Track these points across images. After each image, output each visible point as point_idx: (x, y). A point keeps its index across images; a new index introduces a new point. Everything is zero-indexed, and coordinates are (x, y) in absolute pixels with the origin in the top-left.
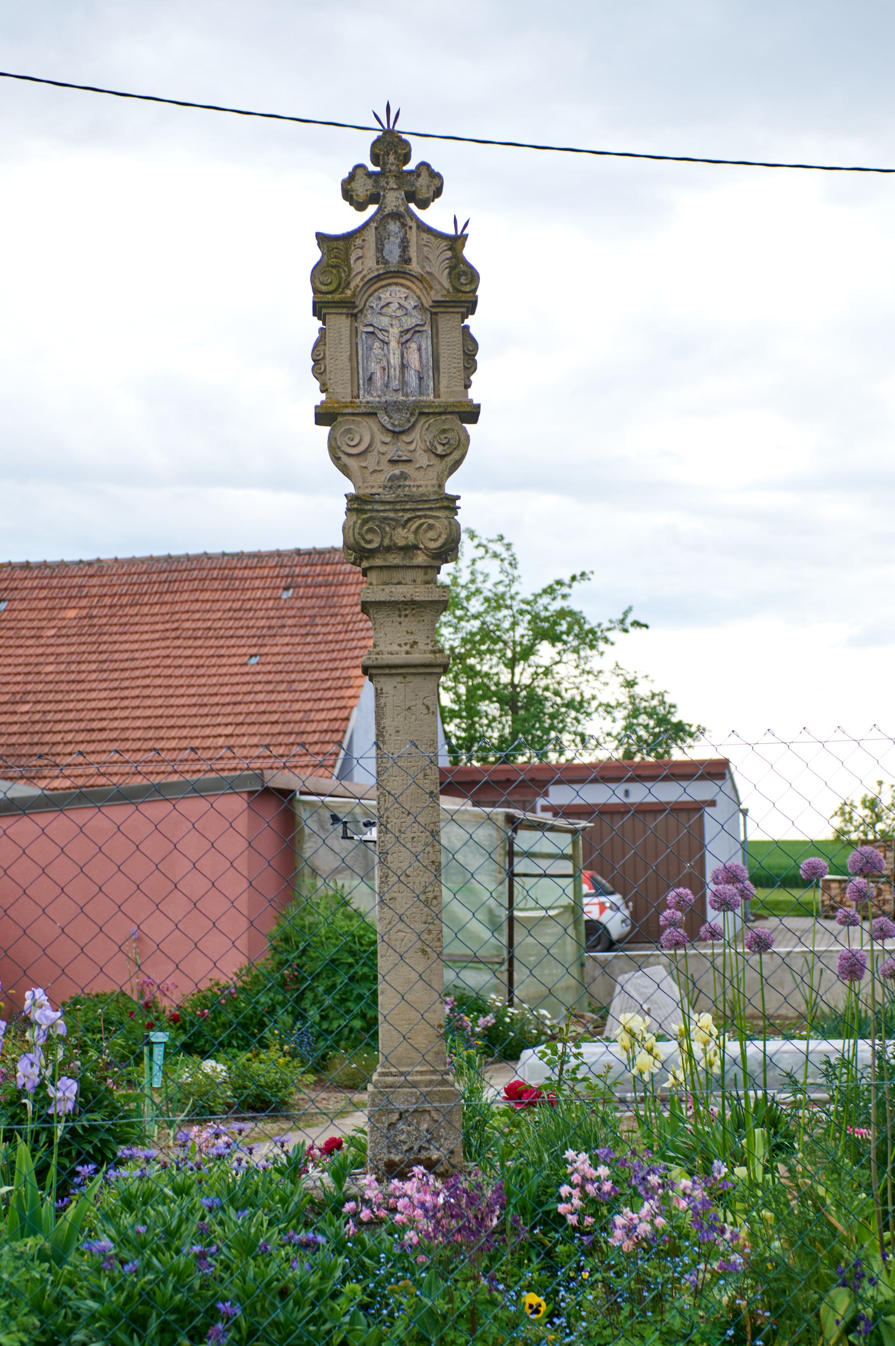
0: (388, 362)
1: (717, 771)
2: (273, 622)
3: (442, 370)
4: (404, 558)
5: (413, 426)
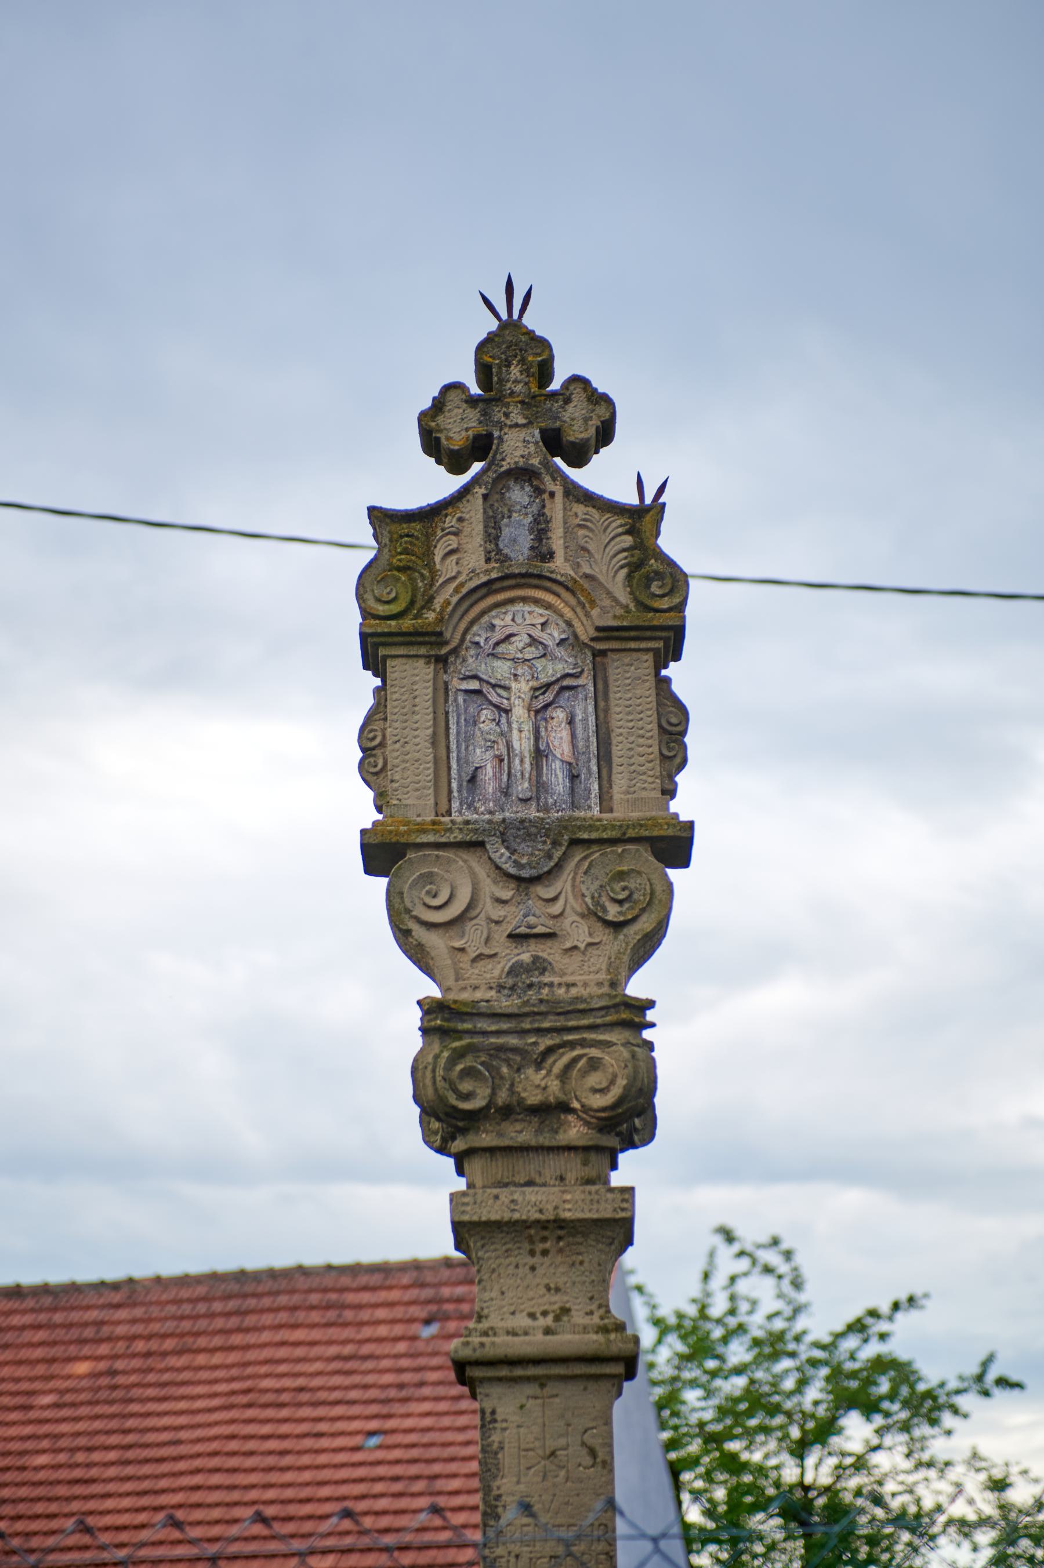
0: (509, 746)
2: (406, 1377)
3: (616, 761)
4: (539, 1131)
5: (559, 866)
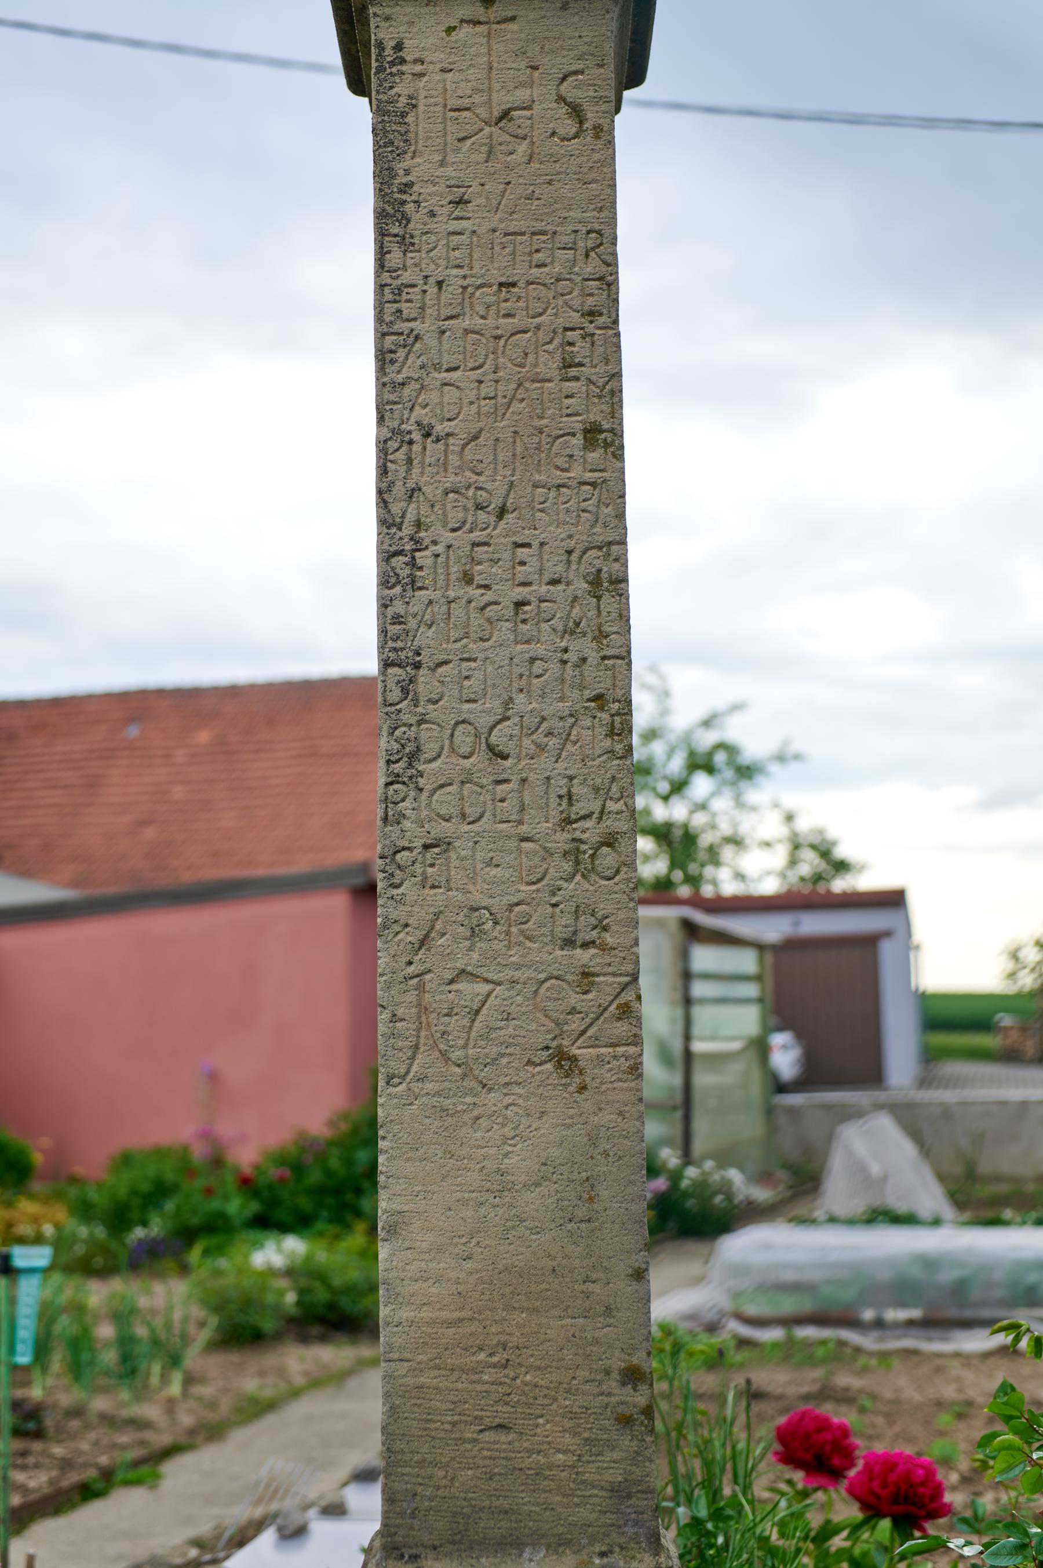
1: (893, 900)
